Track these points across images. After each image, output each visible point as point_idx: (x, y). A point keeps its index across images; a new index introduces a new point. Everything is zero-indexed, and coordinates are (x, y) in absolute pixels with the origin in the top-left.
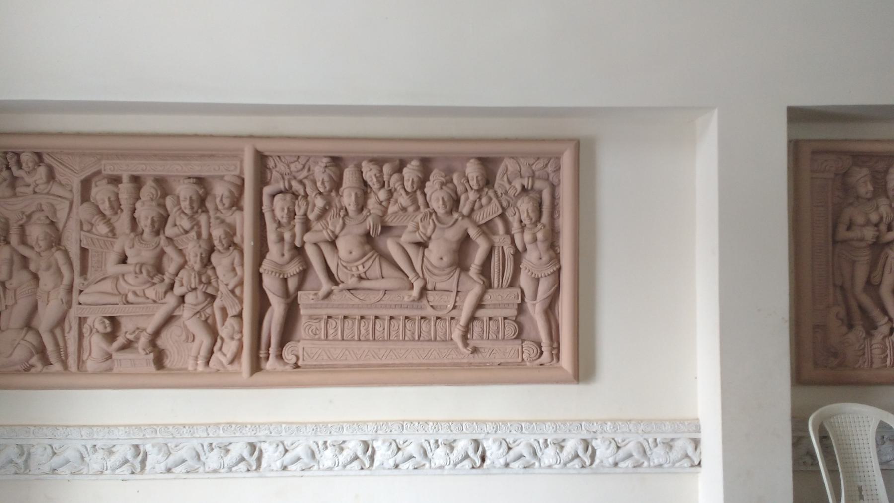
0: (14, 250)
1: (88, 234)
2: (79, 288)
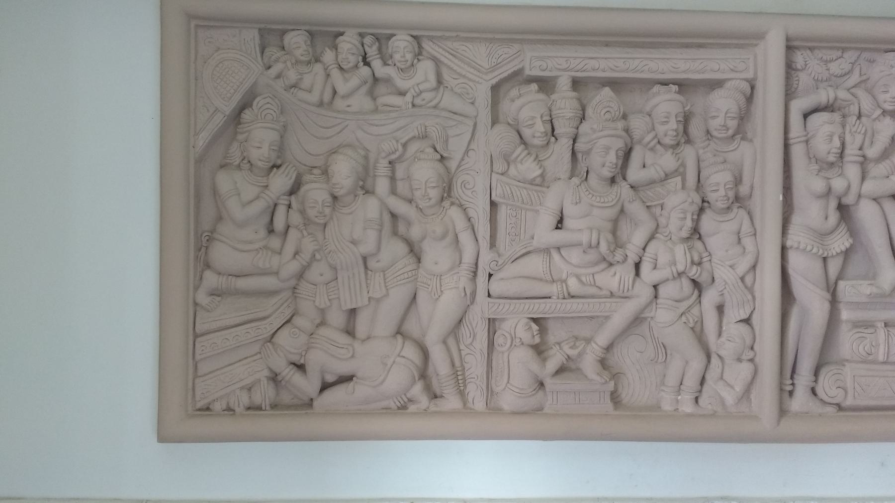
0: (383, 204)
1: (503, 178)
2: (488, 270)
